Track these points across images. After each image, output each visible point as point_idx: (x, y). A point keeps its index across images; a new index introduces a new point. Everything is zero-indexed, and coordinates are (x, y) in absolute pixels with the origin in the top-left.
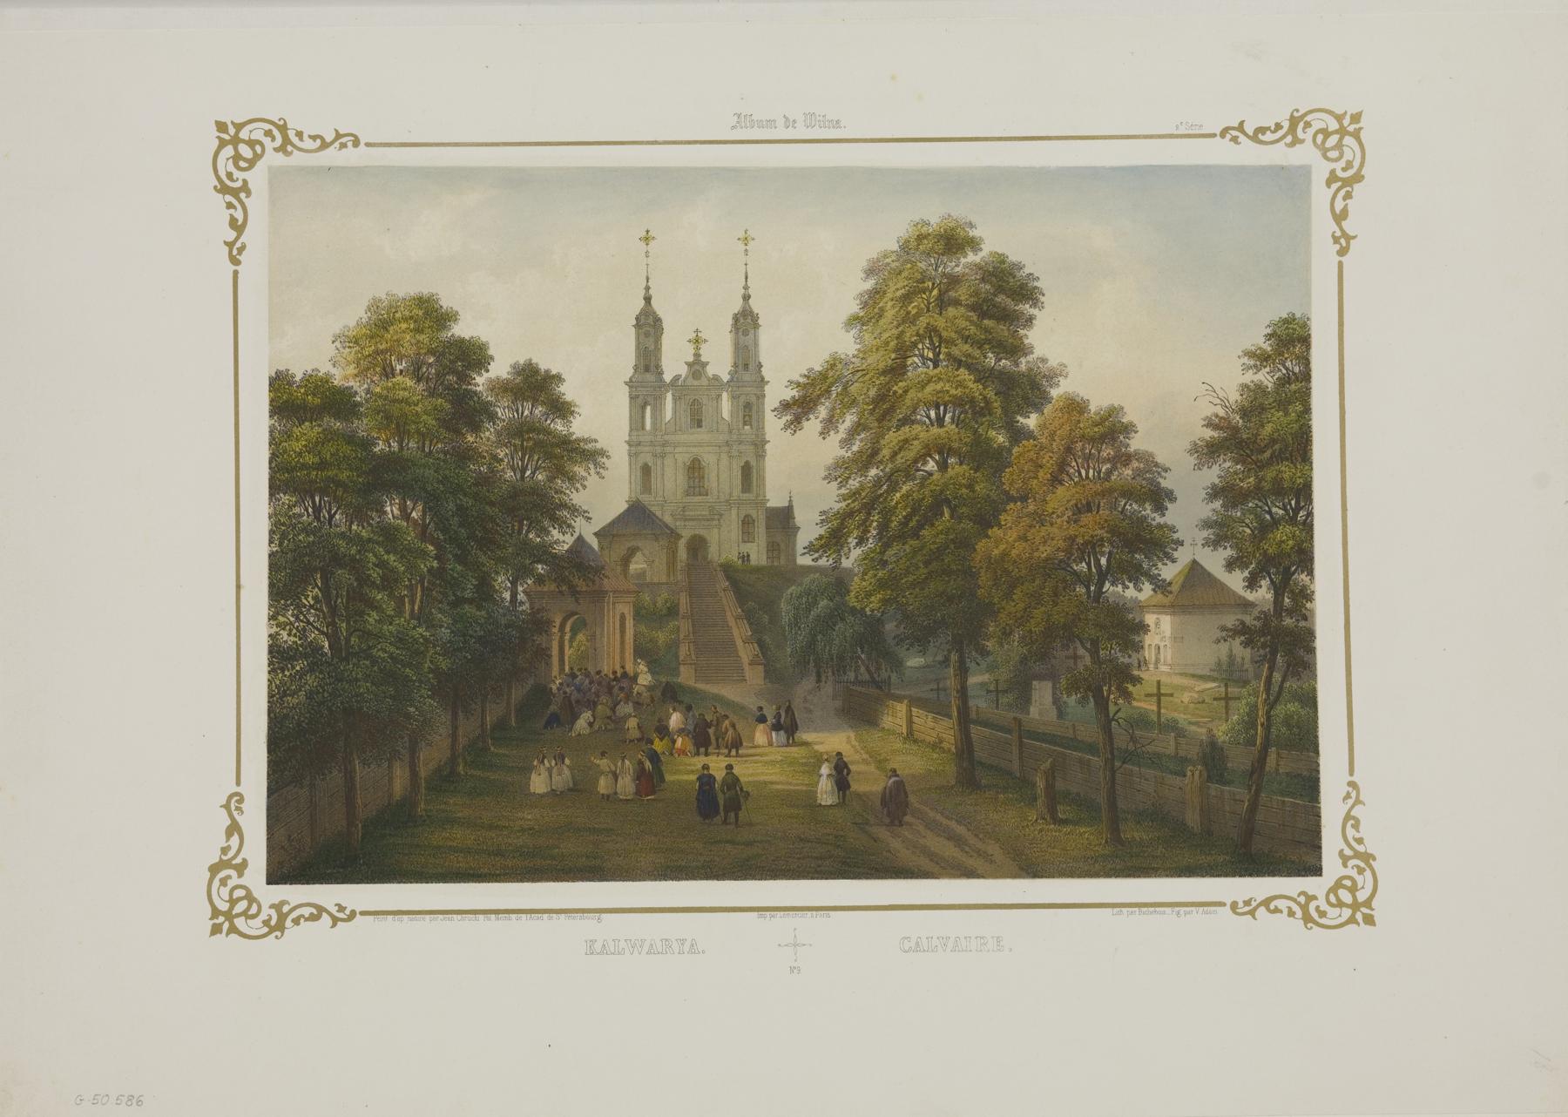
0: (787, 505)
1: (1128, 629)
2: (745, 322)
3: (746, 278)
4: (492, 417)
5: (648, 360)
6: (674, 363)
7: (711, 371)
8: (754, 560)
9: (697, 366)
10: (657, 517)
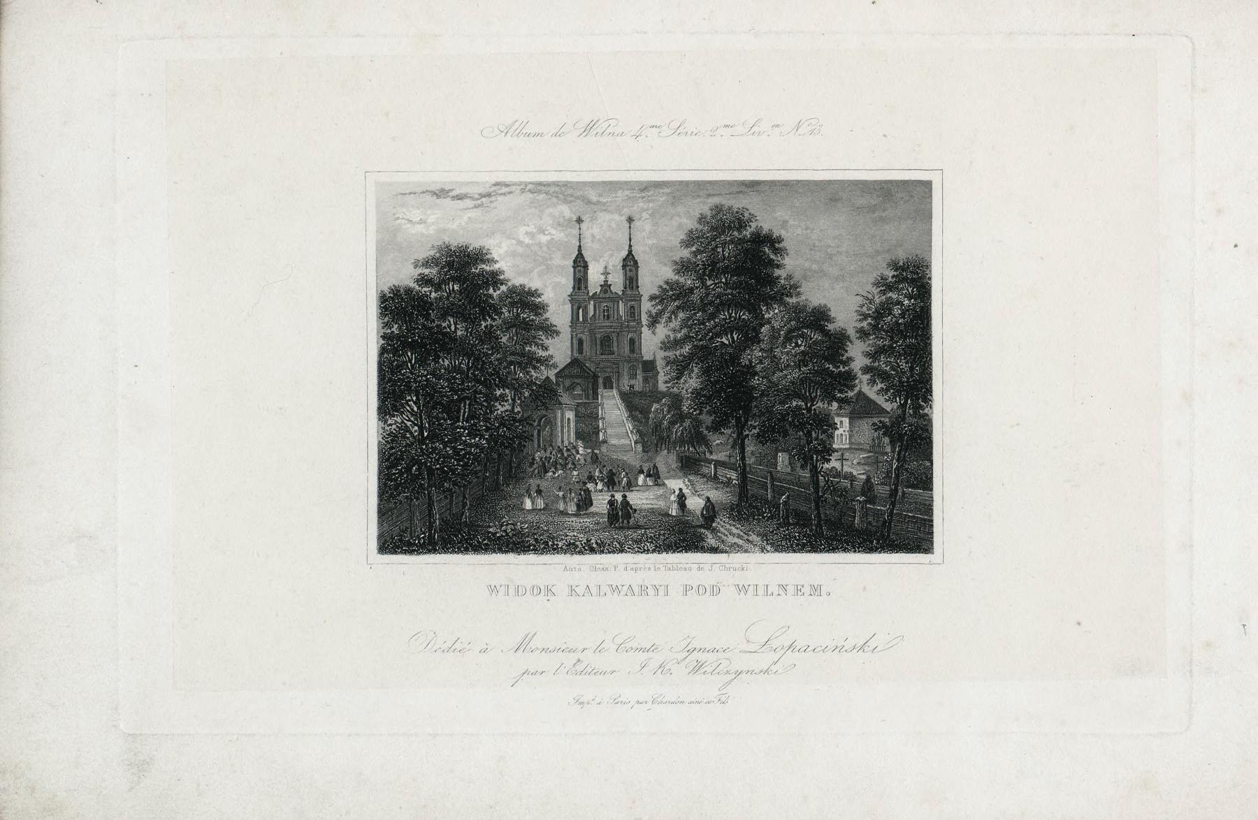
0: (652, 359)
1: (826, 423)
3: (630, 240)
4: (500, 314)
5: (580, 281)
6: (595, 276)
8: (637, 388)
9: (606, 286)
10: (587, 367)
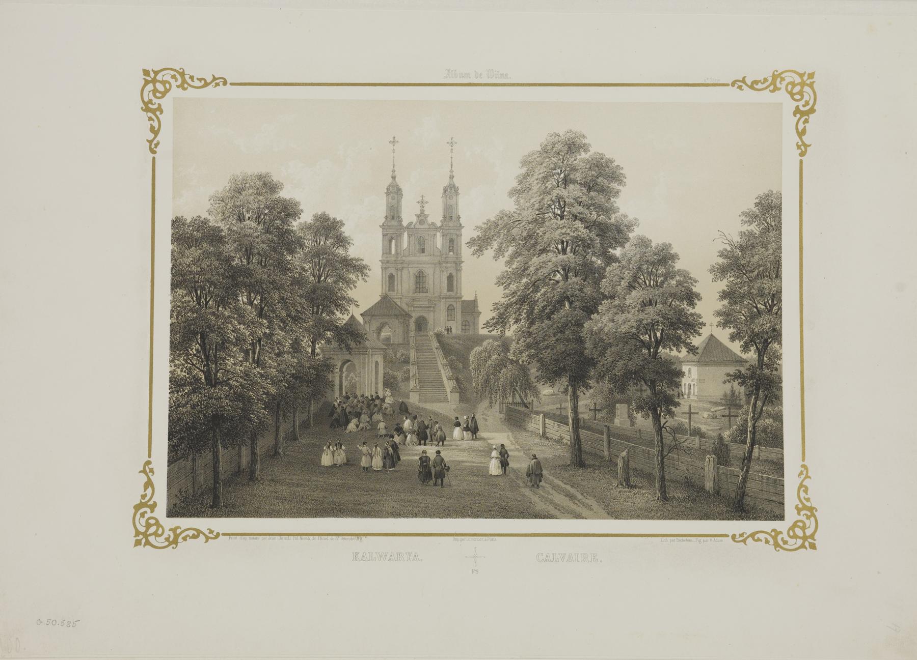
2: (451, 191)
5: (394, 214)
6: (408, 216)
7: (430, 220)
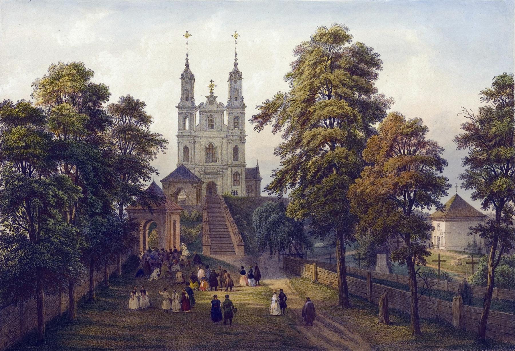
0: (256, 167)
9: (211, 98)
